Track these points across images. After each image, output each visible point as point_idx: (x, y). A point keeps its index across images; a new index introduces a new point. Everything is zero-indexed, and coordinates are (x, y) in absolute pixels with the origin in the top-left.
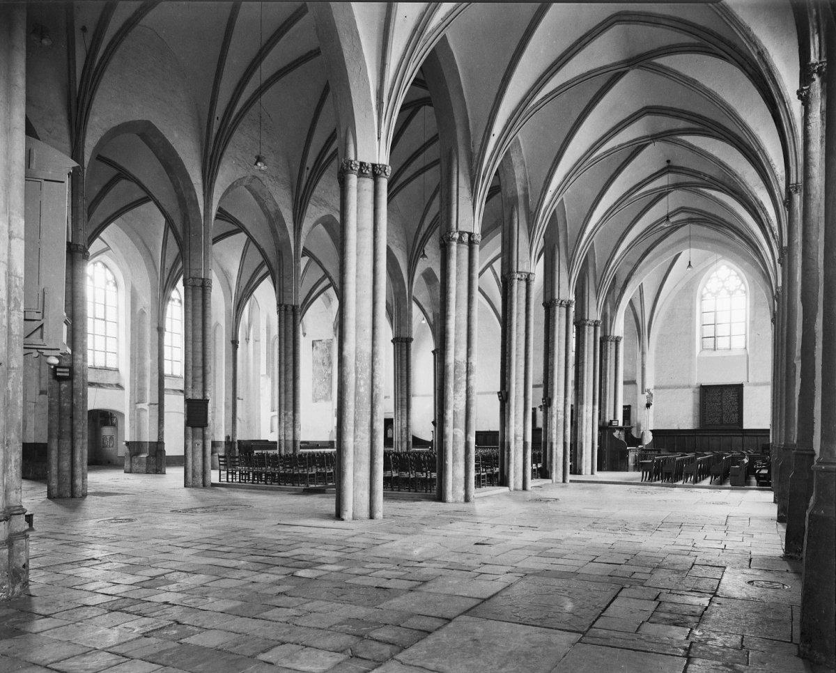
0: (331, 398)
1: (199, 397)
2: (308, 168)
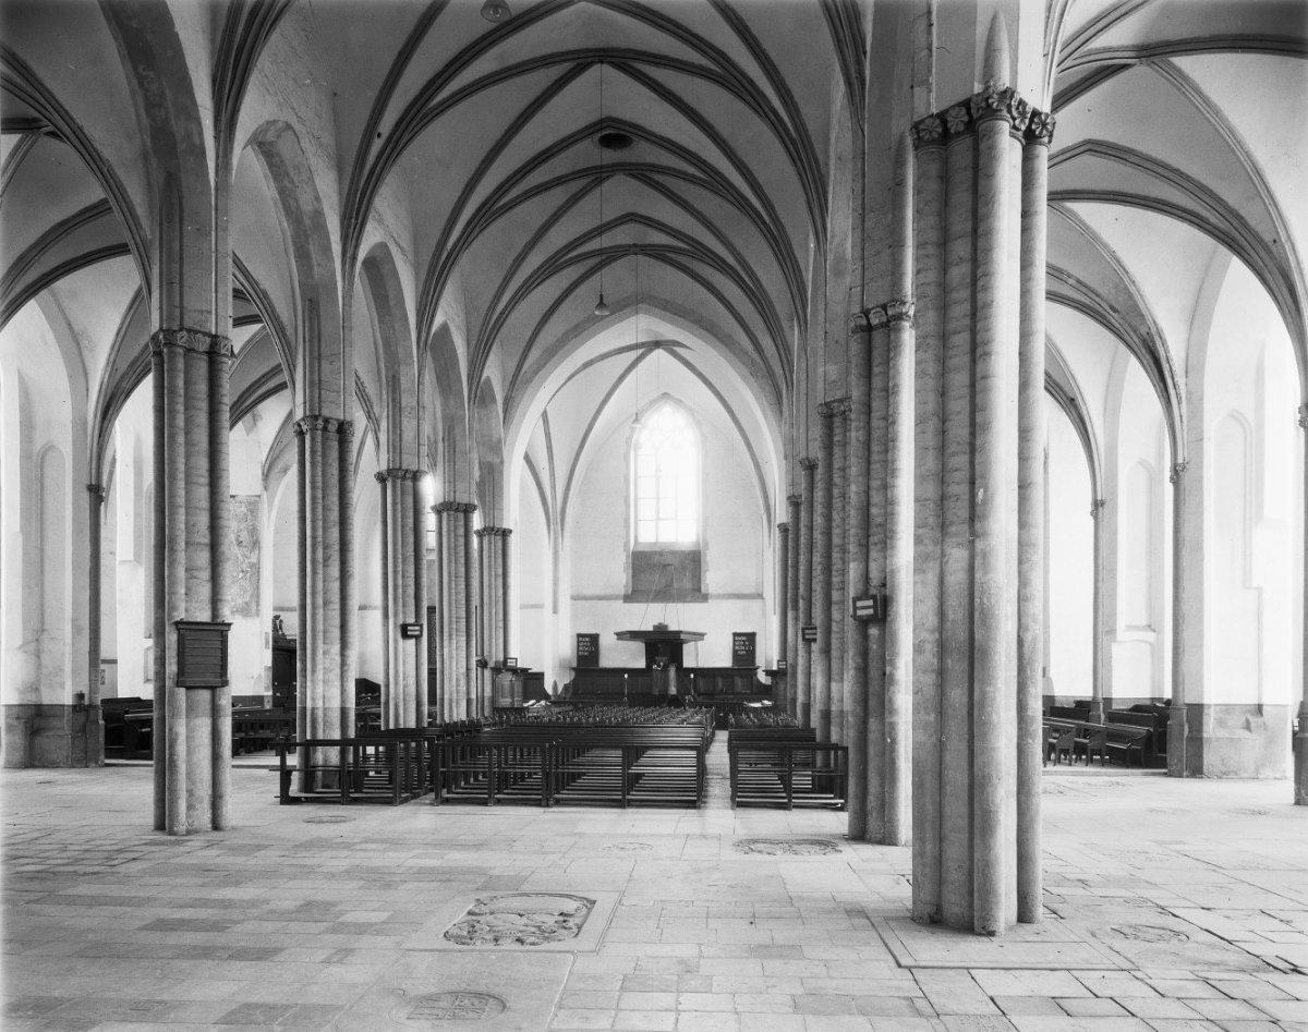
0: (258, 611)
1: (204, 615)
2: (379, 135)
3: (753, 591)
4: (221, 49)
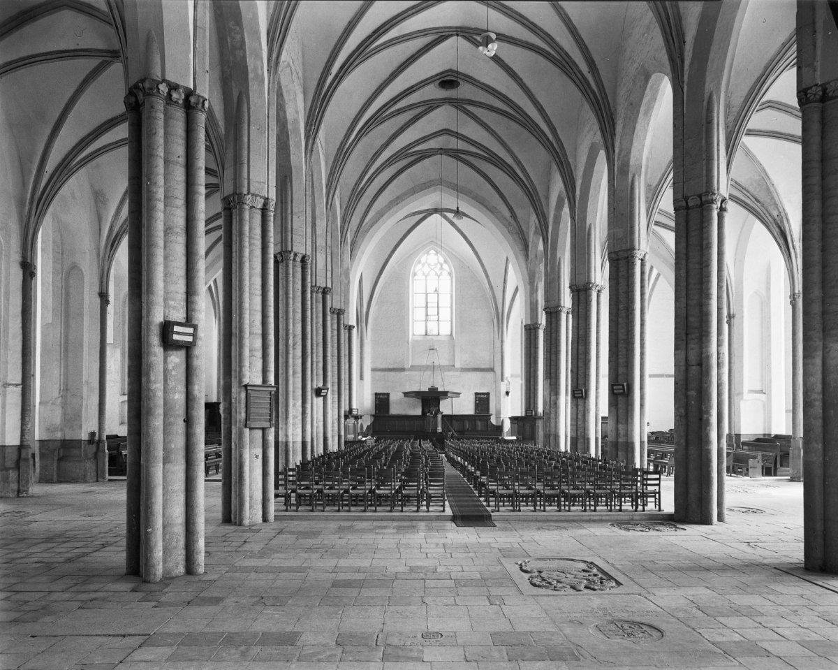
3: (488, 367)
4: (273, 15)
